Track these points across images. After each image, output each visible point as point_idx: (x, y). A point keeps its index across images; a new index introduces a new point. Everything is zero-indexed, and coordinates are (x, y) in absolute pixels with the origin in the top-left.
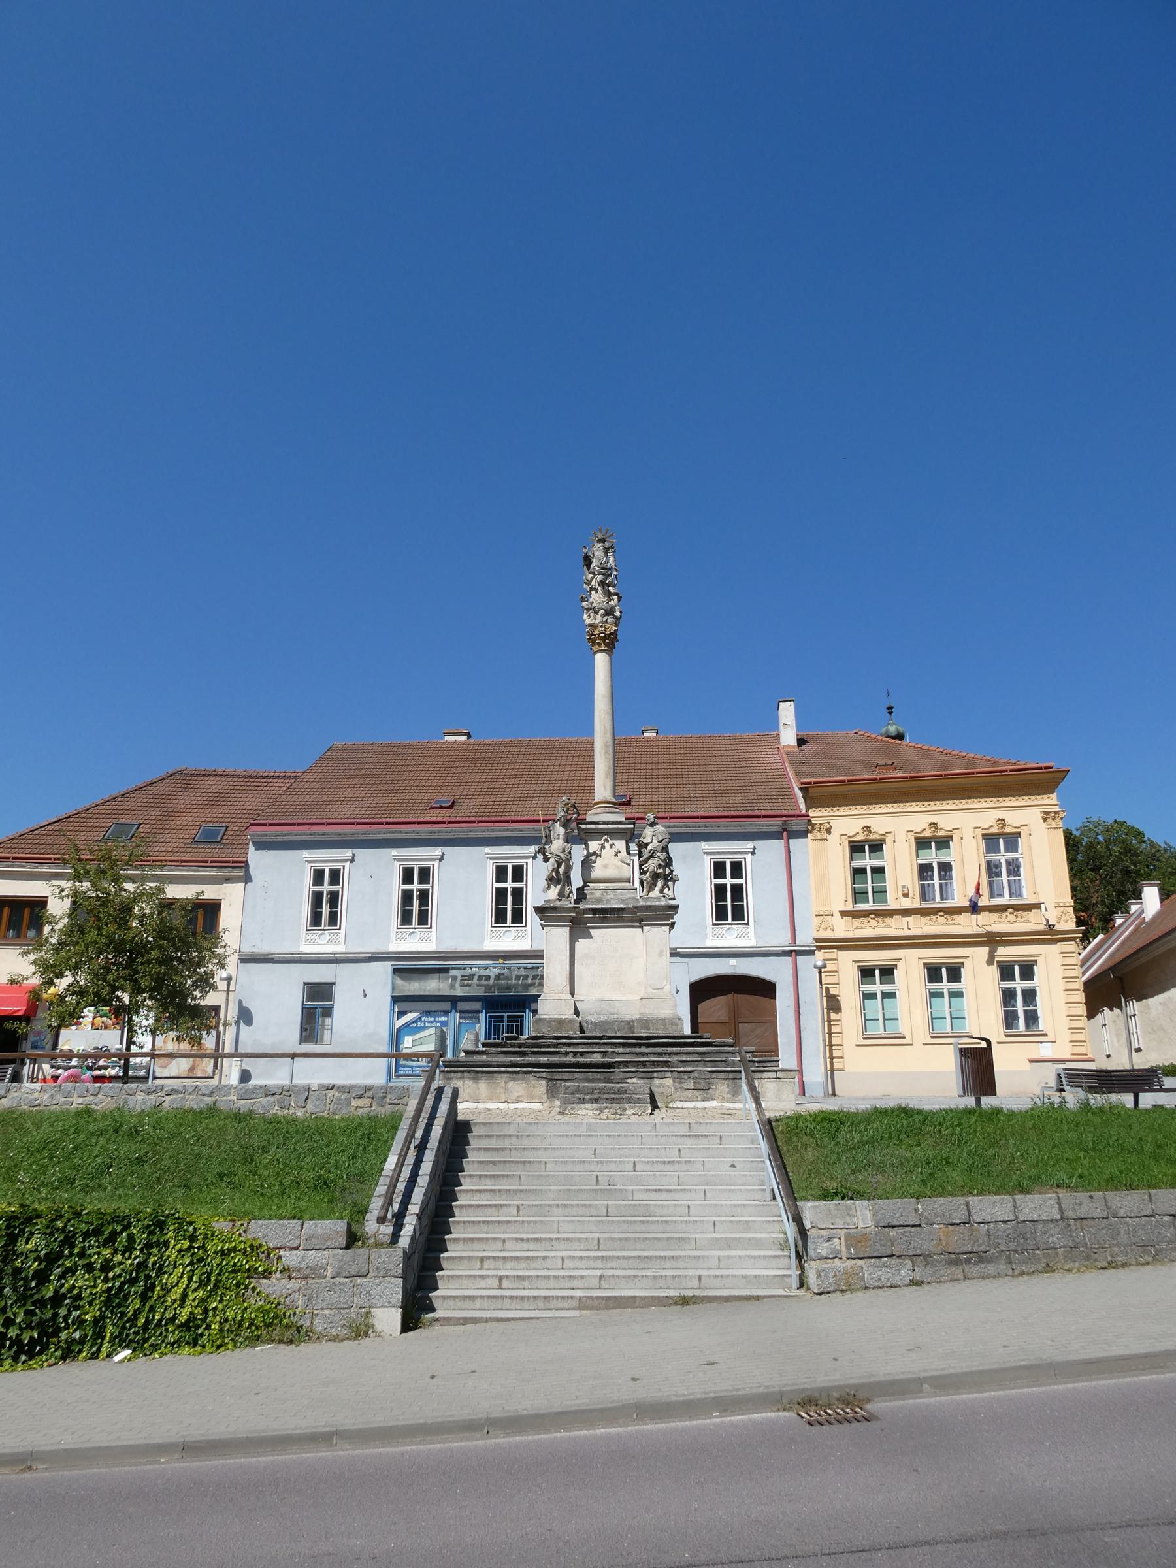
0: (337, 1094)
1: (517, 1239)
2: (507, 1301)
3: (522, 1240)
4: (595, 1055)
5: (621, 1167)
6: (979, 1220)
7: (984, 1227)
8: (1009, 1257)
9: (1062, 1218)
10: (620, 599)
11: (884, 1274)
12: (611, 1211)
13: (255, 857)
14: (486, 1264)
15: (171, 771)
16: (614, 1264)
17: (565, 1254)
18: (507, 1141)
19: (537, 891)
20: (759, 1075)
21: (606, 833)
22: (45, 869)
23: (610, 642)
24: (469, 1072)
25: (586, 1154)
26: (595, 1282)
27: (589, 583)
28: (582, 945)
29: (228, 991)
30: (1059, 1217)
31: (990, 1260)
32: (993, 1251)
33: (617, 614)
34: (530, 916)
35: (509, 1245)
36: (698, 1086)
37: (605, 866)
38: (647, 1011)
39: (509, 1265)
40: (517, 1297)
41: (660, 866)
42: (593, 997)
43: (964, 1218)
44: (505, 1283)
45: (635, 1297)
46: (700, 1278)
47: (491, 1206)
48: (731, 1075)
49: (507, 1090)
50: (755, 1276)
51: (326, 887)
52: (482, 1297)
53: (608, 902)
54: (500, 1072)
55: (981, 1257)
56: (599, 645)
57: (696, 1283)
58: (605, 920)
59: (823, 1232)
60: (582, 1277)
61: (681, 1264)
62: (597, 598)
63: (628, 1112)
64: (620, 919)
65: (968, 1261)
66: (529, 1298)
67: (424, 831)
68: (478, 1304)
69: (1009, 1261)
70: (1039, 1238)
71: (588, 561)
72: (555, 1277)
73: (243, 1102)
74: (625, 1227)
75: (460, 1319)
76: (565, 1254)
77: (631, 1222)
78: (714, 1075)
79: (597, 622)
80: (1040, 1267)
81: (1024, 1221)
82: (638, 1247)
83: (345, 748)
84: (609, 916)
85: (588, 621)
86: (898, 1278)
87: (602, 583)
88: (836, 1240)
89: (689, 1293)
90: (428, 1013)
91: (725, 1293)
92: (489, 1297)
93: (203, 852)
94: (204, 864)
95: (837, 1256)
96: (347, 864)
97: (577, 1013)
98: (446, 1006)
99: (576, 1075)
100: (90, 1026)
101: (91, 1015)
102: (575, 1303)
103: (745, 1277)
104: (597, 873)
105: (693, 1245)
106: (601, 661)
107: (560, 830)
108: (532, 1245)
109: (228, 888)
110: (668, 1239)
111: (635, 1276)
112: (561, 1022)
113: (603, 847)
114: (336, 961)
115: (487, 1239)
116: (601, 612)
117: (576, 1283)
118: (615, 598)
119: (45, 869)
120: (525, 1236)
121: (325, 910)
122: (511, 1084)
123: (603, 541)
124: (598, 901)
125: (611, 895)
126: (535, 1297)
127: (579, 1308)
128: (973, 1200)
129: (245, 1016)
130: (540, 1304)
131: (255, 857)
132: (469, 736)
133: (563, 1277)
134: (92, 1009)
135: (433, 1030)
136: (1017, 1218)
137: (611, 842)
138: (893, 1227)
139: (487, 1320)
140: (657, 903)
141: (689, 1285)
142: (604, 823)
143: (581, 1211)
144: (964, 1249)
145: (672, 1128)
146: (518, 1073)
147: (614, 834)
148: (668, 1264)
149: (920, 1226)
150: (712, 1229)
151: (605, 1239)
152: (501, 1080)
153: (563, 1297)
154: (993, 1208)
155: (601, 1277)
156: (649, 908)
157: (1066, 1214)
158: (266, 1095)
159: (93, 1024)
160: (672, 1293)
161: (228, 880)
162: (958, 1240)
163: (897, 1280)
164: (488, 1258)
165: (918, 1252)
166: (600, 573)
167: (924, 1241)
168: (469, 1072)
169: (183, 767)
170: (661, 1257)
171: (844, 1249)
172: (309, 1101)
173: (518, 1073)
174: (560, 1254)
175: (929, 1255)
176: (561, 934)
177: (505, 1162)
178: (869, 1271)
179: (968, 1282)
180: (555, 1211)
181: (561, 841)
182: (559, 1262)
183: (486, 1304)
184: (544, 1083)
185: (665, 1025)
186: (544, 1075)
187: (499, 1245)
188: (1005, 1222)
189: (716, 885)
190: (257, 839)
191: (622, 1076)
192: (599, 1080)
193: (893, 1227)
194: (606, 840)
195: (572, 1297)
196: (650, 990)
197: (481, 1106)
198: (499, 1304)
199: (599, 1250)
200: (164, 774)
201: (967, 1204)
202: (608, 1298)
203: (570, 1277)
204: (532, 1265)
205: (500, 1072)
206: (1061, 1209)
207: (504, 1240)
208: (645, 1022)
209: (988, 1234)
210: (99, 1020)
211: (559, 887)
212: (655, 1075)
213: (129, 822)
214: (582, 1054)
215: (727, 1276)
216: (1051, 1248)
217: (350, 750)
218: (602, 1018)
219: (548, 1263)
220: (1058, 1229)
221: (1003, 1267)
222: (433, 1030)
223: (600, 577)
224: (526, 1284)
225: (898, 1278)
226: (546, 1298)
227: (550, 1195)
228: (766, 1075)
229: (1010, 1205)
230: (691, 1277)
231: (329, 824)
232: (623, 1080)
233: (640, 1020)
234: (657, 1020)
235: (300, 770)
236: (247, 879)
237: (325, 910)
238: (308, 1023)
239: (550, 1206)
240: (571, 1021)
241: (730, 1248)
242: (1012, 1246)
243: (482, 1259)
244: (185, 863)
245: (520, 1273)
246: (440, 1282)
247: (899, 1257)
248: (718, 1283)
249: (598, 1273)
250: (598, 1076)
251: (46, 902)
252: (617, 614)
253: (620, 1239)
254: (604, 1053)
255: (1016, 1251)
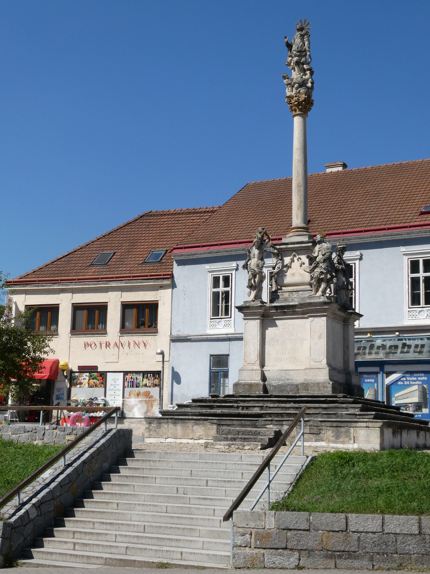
0: (58, 432)
1: (101, 523)
2: (68, 557)
3: (103, 523)
4: (256, 409)
5: (199, 483)
6: (354, 530)
7: (356, 535)
8: (372, 557)
9: (420, 533)
10: (312, 73)
11: (278, 560)
12: (169, 510)
13: (178, 271)
14: (76, 536)
15: (141, 214)
16: (144, 541)
17: (118, 533)
18: (147, 463)
19: (241, 294)
20: (354, 424)
21: (294, 251)
22: (56, 287)
23: (304, 107)
24: (171, 419)
25: (185, 474)
26: (123, 551)
27: (289, 64)
28: (270, 332)
29: (163, 361)
30: (417, 532)
31: (357, 558)
32: (360, 552)
33: (309, 85)
34: (234, 311)
35: (96, 525)
36: (312, 431)
37: (293, 275)
38: (309, 378)
39: (88, 537)
40: (74, 555)
41: (322, 273)
42: (276, 368)
43: (343, 527)
44: (77, 547)
45: (135, 561)
46: (182, 553)
47: (103, 502)
48: (335, 424)
49: (193, 431)
50: (214, 555)
51: (221, 289)
52: (56, 553)
53: (293, 300)
54: (189, 419)
55: (350, 555)
56: (295, 110)
57: (179, 556)
58: (285, 314)
59: (240, 530)
60: (117, 547)
61: (181, 544)
62: (295, 75)
63: (246, 448)
64: (294, 313)
65: (340, 557)
66: (79, 556)
67: (416, 233)
68: (54, 557)
69: (372, 559)
70: (398, 546)
71: (289, 46)
72: (103, 546)
73: (14, 435)
74: (168, 520)
75: (36, 564)
76: (118, 533)
77: (172, 517)
78: (323, 424)
79: (293, 93)
80: (395, 565)
81: (388, 533)
82: (166, 532)
83: (256, 185)
84: (289, 311)
85: (288, 94)
86: (287, 563)
87: (298, 63)
88: (248, 535)
89: (165, 561)
90: (412, 373)
91: (196, 564)
92: (60, 554)
93: (148, 270)
94: (146, 278)
95: (248, 545)
96: (357, 262)
97: (264, 378)
98: (376, 369)
99: (235, 422)
100: (87, 385)
101: (87, 378)
102: (103, 561)
103: (208, 555)
104: (288, 279)
105: (198, 534)
106: (297, 121)
107: (255, 251)
108: (108, 527)
109: (162, 292)
110: (184, 529)
111: (146, 549)
112: (251, 385)
113: (293, 261)
114: (229, 339)
115: (85, 521)
116: (296, 85)
117: (113, 550)
118: (308, 72)
119: (56, 287)
120: (105, 521)
121: (222, 305)
122: (195, 427)
123: (301, 29)
124: (286, 300)
125: (295, 295)
126: (82, 556)
127: (105, 564)
128: (352, 517)
129: (176, 378)
130: (85, 560)
131: (178, 271)
132: (344, 166)
133: (107, 546)
134: (88, 374)
135: (416, 387)
136: (383, 530)
137: (297, 257)
138: (290, 530)
139: (49, 566)
140: (318, 300)
141: (175, 557)
142: (292, 243)
143: (152, 508)
144: (339, 548)
145: (251, 459)
146: (199, 420)
147: (299, 251)
148: (174, 544)
149: (309, 530)
150: (219, 525)
151: (148, 526)
152: (190, 424)
153: (97, 557)
154: (366, 522)
155: (127, 548)
156: (310, 304)
157: (423, 531)
158: (25, 432)
159: (89, 384)
160: (156, 560)
161: (162, 287)
162: (336, 542)
163: (286, 564)
164: (77, 532)
165: (305, 548)
166: (296, 56)
167: (310, 540)
168: (171, 419)
169: (150, 210)
170: (170, 539)
171: (253, 540)
172: (45, 436)
173: (199, 420)
174: (115, 533)
175: (313, 550)
176: (254, 325)
177: (133, 476)
178: (270, 558)
179: (336, 570)
180: (137, 507)
181: (256, 259)
182: (114, 537)
183: (58, 557)
184: (215, 427)
185: (319, 388)
186: (215, 421)
187: (91, 525)
188: (374, 533)
189: (412, 279)
190: (178, 258)
191: (263, 423)
192: (249, 426)
193: (290, 530)
194: (295, 256)
195: (102, 558)
196: (312, 363)
197: (178, 441)
198: (64, 558)
199: (144, 532)
200: (136, 216)
201: (347, 519)
202: (121, 560)
203: (110, 546)
204: (141, 542)
205: (189, 419)
206: (420, 527)
207: (94, 523)
208: (306, 386)
209: (359, 539)
210: (92, 381)
211: (255, 291)
212: (284, 423)
213: (109, 252)
214: (247, 408)
215: (197, 554)
216: (407, 554)
217: (258, 186)
218: (281, 382)
219: (108, 538)
220: (414, 541)
221: (365, 563)
222: (416, 387)
223: (295, 59)
224: (87, 548)
225: (287, 563)
226: (88, 557)
227: (143, 498)
228: (359, 424)
229: (380, 522)
230: (176, 552)
231: (221, 245)
232: (264, 426)
233: (302, 384)
234: (314, 384)
235: (216, 206)
236: (173, 286)
237: (222, 305)
238: (214, 382)
239: (135, 504)
240: (257, 385)
241: (219, 537)
242: (376, 549)
243: (74, 533)
244: (135, 278)
245: (85, 542)
246: (45, 544)
247: (291, 550)
248: (192, 557)
249: (126, 545)
250: (248, 423)
251: (58, 308)
252: (309, 85)
253: (157, 527)
254: (261, 407)
255: (378, 553)
